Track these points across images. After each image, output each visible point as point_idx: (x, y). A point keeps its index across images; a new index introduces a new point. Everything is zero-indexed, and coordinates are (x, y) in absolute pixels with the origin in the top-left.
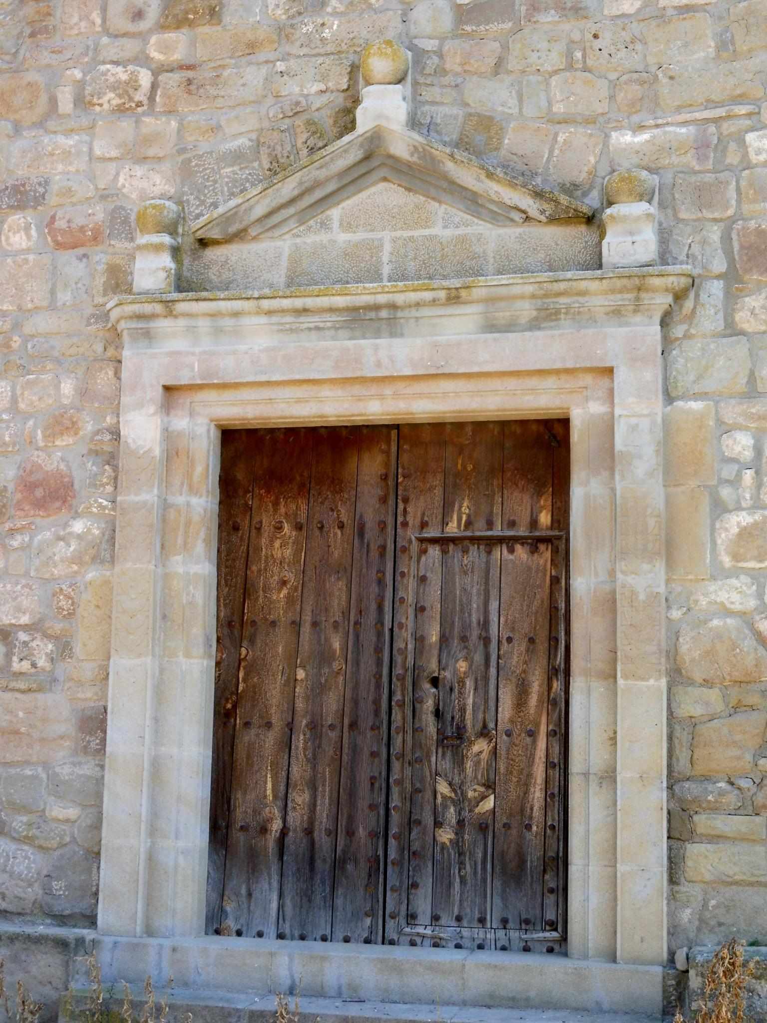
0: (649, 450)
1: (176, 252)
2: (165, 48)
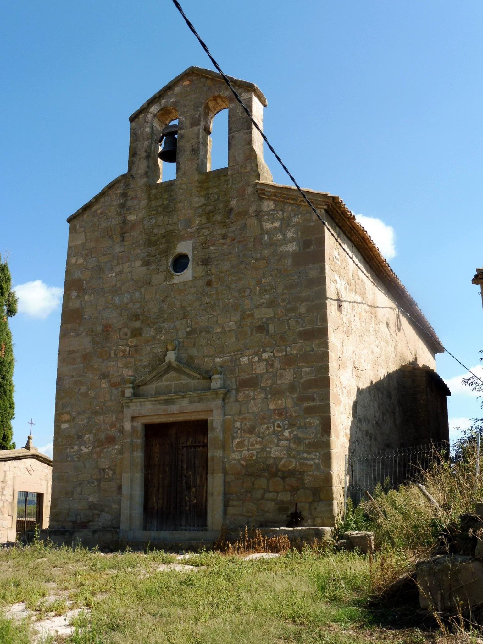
0: (219, 427)
1: (133, 388)
2: (131, 342)
